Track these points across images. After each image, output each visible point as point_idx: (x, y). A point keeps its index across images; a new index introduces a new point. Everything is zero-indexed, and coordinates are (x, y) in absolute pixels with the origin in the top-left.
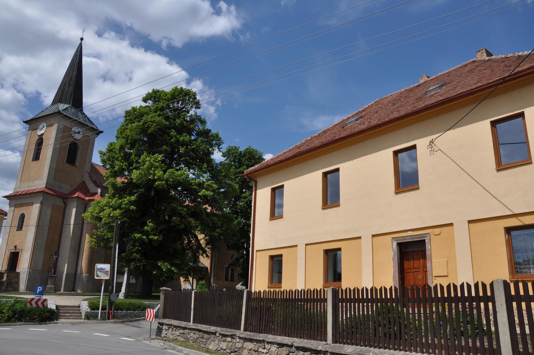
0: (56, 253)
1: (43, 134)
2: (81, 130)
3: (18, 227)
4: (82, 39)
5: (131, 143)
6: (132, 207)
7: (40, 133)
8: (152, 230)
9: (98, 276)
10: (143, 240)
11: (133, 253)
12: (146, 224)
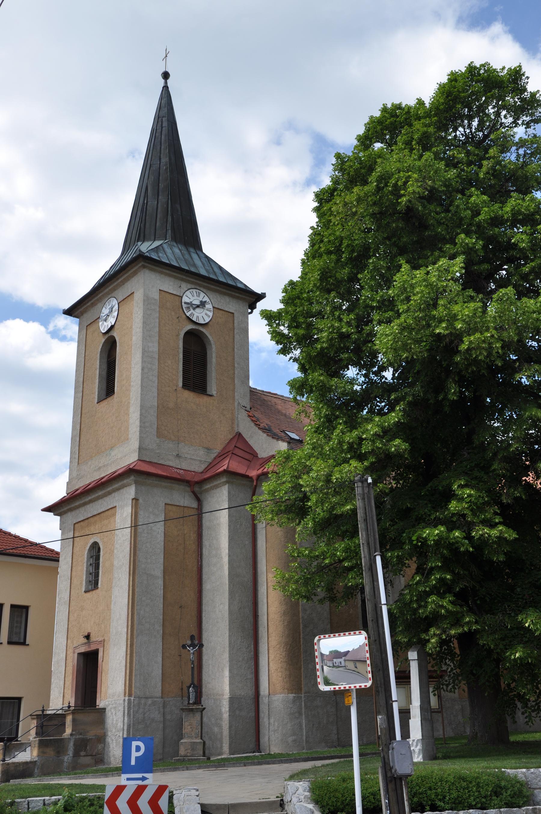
0: (192, 638)
1: (112, 327)
2: (206, 299)
3: (89, 582)
4: (166, 76)
5: (350, 260)
6: (398, 445)
7: (104, 327)
8: (477, 508)
9: (327, 682)
10: (453, 547)
11: (427, 594)
12: (449, 495)
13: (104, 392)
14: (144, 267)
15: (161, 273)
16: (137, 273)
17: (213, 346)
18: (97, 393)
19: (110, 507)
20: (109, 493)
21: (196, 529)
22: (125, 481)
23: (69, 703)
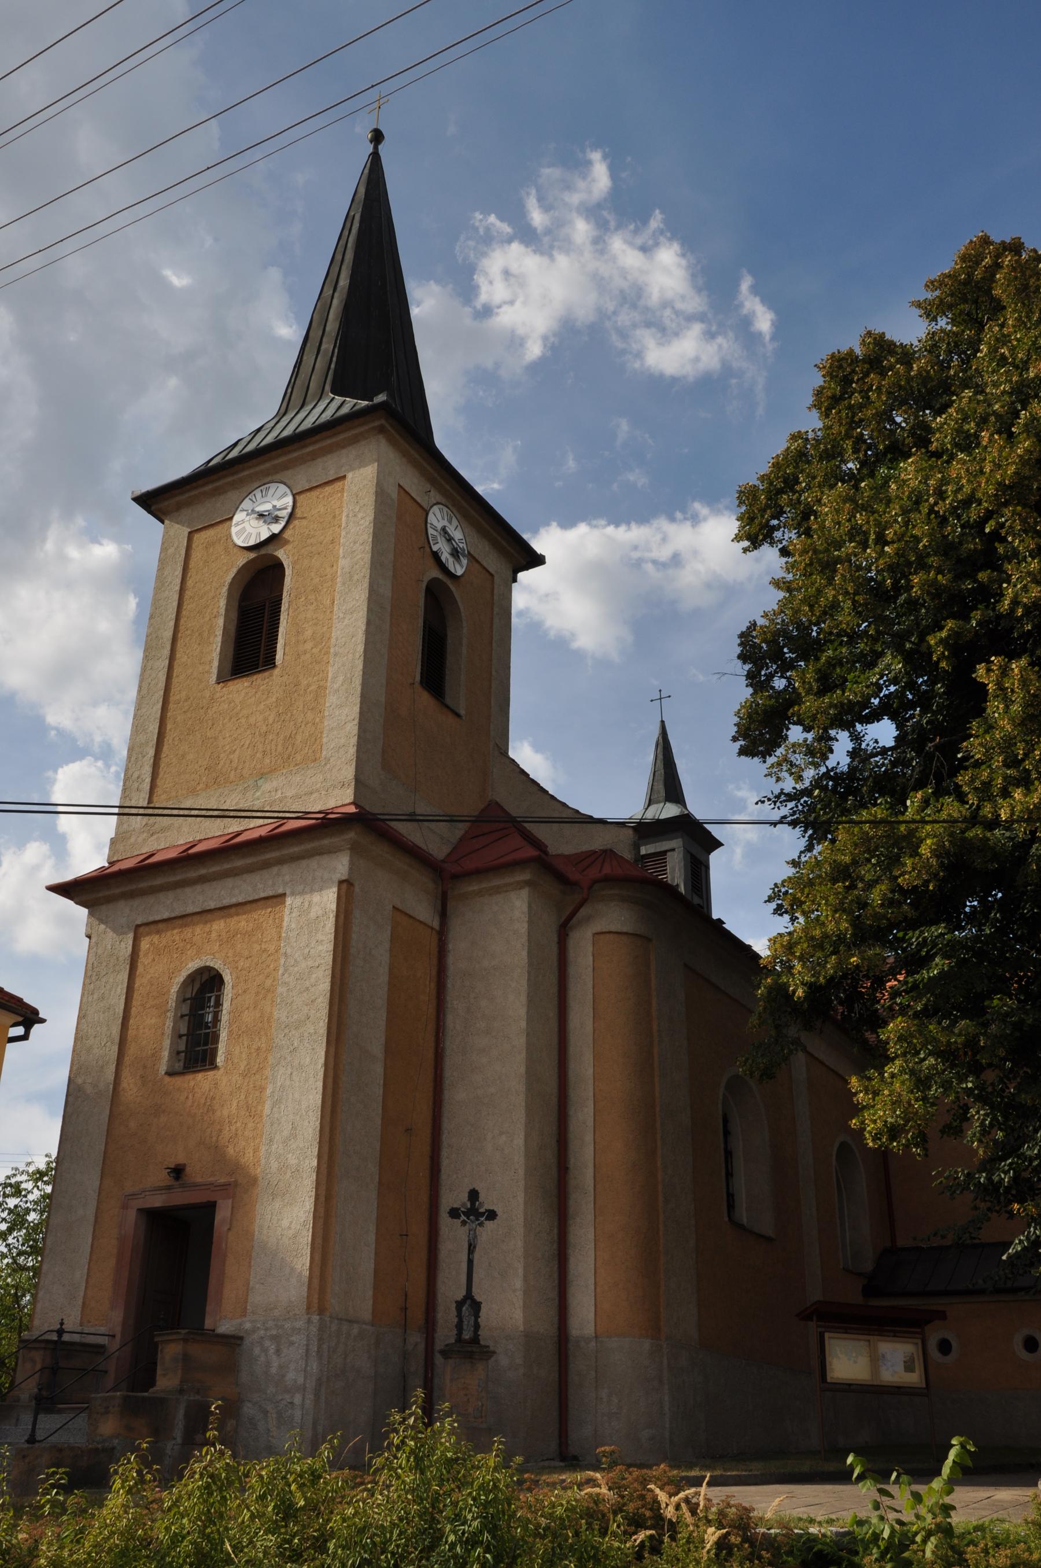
4: (377, 137)
13: (229, 666)
14: (381, 430)
15: (404, 454)
16: (358, 441)
17: (465, 624)
18: (216, 664)
19: (262, 895)
20: (266, 865)
21: (434, 972)
22: (326, 842)
23: (62, 1324)
